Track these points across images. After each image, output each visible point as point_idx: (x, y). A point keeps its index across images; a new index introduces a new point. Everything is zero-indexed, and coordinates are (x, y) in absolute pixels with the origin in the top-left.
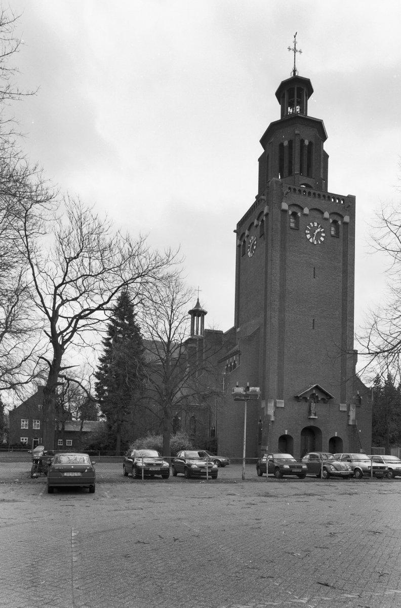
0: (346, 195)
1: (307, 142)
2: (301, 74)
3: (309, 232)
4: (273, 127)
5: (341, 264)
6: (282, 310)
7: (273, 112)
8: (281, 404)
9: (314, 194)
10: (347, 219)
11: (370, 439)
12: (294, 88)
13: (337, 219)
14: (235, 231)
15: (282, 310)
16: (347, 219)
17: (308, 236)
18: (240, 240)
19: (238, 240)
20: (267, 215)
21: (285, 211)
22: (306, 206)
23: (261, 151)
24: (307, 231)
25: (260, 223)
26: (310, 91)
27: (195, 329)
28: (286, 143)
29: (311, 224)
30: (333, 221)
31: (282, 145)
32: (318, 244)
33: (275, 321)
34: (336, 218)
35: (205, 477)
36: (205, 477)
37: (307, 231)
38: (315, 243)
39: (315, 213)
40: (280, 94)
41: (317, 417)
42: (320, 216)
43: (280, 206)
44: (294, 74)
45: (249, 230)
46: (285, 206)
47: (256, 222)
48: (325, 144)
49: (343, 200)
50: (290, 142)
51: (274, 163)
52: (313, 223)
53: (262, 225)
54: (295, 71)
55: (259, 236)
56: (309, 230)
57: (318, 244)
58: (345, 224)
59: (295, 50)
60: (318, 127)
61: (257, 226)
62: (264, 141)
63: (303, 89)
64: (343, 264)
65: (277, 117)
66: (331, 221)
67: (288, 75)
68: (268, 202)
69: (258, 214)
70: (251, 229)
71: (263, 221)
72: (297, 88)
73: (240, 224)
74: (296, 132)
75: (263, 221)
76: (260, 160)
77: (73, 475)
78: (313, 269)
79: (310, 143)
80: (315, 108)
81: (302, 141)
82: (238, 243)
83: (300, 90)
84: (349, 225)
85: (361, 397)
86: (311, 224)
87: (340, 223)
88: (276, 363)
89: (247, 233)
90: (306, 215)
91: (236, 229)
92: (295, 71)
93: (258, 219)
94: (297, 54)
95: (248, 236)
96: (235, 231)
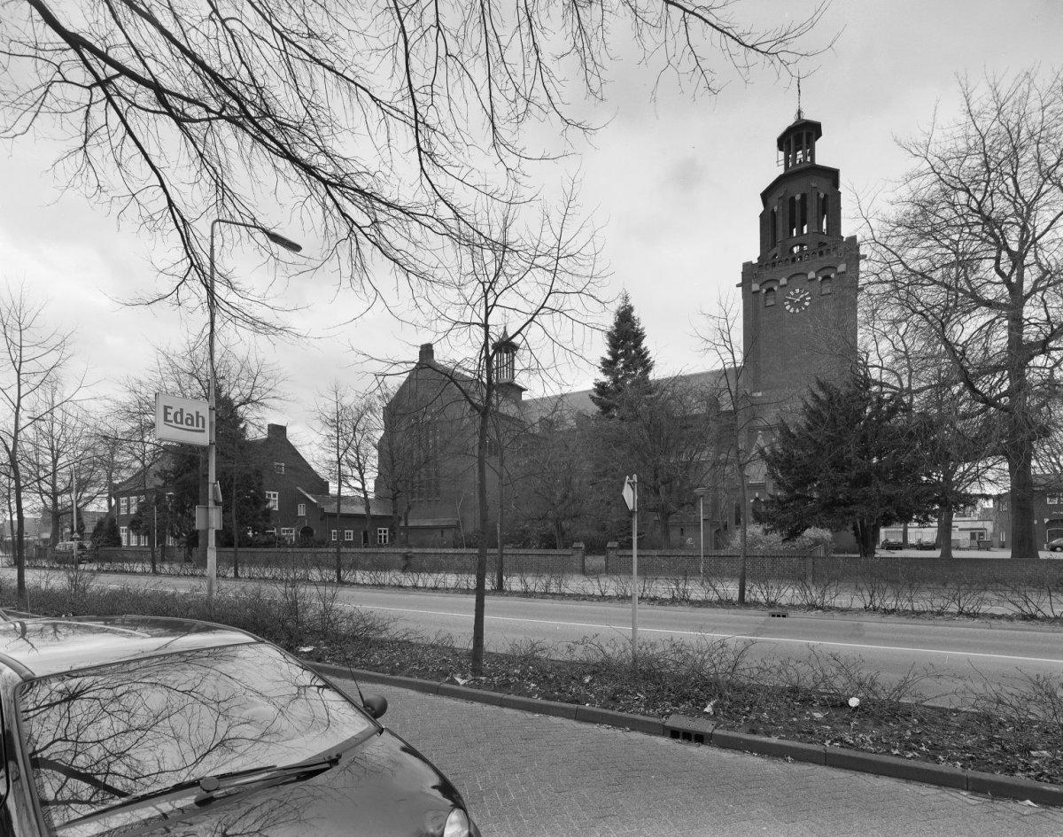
1: (822, 195)
2: (807, 116)
7: (772, 166)
11: (275, 423)
12: (802, 134)
17: (807, 304)
26: (819, 134)
28: (798, 197)
31: (793, 198)
35: (628, 553)
36: (628, 553)
40: (780, 147)
44: (799, 117)
50: (804, 196)
52: (794, 291)
54: (799, 112)
65: (781, 171)
67: (790, 120)
74: (813, 185)
80: (825, 153)
83: (809, 135)
85: (1046, 520)
92: (799, 112)
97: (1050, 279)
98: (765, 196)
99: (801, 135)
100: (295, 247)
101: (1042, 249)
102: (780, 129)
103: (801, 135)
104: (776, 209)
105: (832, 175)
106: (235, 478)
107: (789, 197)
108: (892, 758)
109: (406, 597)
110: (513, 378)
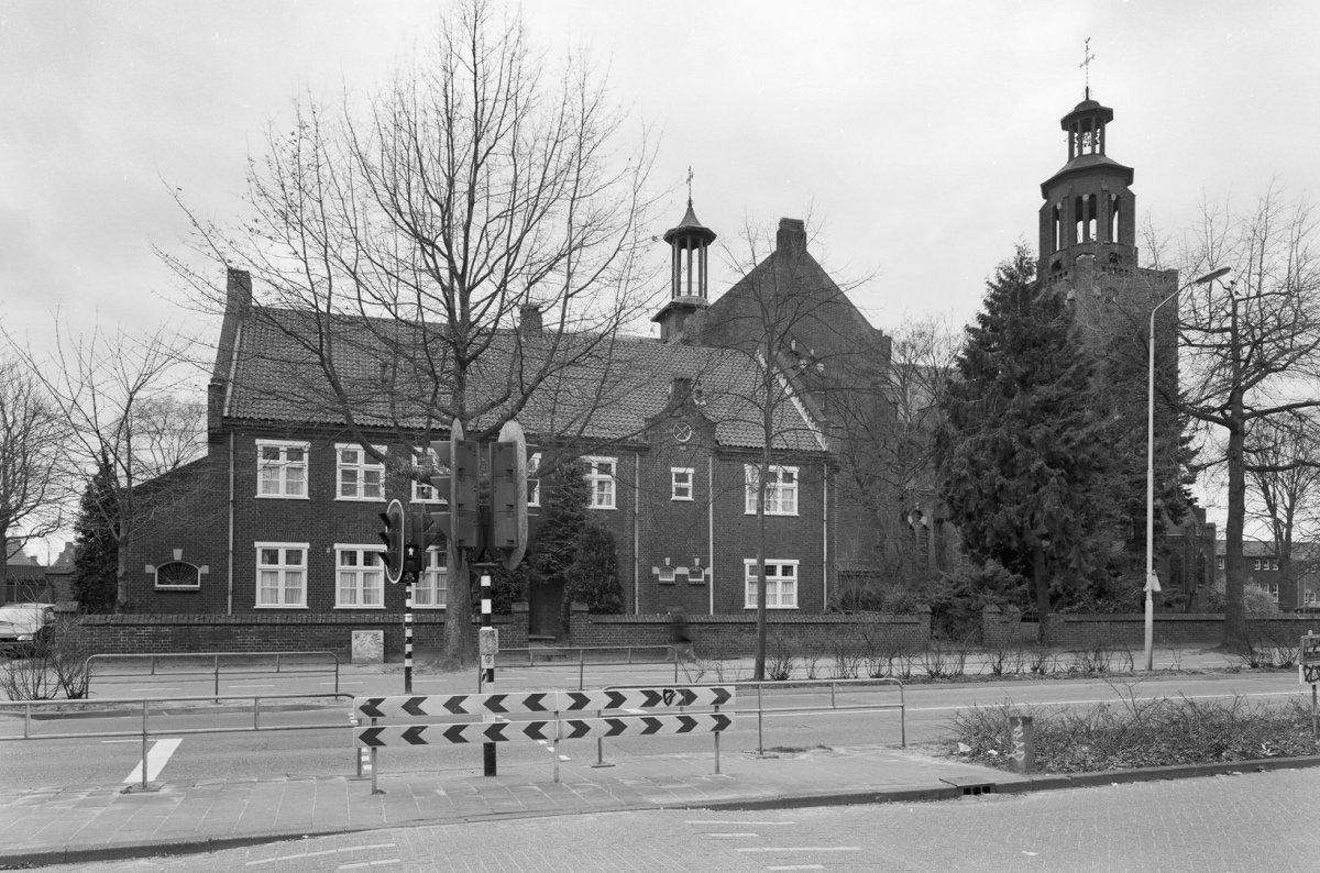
1: (1114, 197)
7: (1055, 155)
28: (1086, 198)
40: (1064, 128)
50: (1092, 197)
74: (1105, 187)
80: (1118, 145)
97: (117, 459)
98: (1047, 188)
99: (1088, 119)
100: (490, 769)
101: (178, 462)
102: (1069, 108)
103: (1088, 119)
104: (1059, 206)
105: (1126, 174)
106: (404, 88)
107: (1076, 196)
108: (525, 458)
109: (1056, 687)
110: (1156, 256)
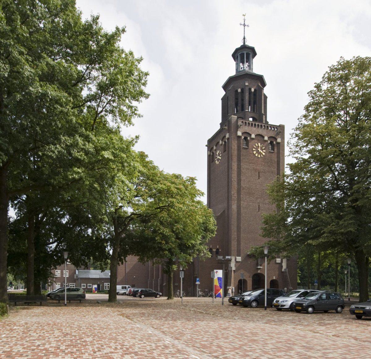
0: (278, 125)
2: (249, 43)
3: (255, 149)
4: (231, 80)
5: (276, 169)
6: (239, 199)
8: (239, 259)
9: (258, 125)
10: (279, 140)
12: (244, 53)
13: (250, 53)
14: (206, 146)
15: (239, 199)
16: (279, 140)
18: (210, 151)
19: (209, 152)
20: (228, 139)
21: (239, 137)
22: (253, 133)
23: (223, 93)
24: (254, 149)
25: (224, 143)
27: (318, 312)
28: (239, 90)
29: (256, 144)
30: (270, 142)
32: (261, 157)
33: (234, 207)
34: (272, 140)
37: (254, 149)
38: (259, 156)
39: (259, 138)
41: (262, 267)
42: (262, 138)
43: (236, 133)
45: (216, 146)
46: (239, 133)
47: (221, 142)
48: (265, 88)
49: (277, 128)
51: (232, 102)
53: (225, 145)
55: (223, 151)
56: (255, 148)
57: (261, 157)
58: (278, 143)
59: (244, 25)
60: (260, 80)
61: (221, 145)
62: (225, 87)
63: (250, 54)
64: (277, 169)
65: (233, 73)
66: (269, 142)
67: (239, 44)
68: (229, 131)
69: (222, 137)
70: (218, 146)
71: (225, 142)
72: (246, 53)
73: (210, 141)
75: (225, 142)
76: (222, 99)
77: (367, 317)
78: (258, 173)
79: (255, 90)
81: (250, 89)
82: (209, 154)
84: (281, 144)
86: (256, 144)
87: (275, 143)
88: (236, 233)
89: (215, 148)
90: (253, 139)
91: (207, 144)
93: (222, 140)
94: (243, 23)
95: (215, 150)
96: (206, 146)
